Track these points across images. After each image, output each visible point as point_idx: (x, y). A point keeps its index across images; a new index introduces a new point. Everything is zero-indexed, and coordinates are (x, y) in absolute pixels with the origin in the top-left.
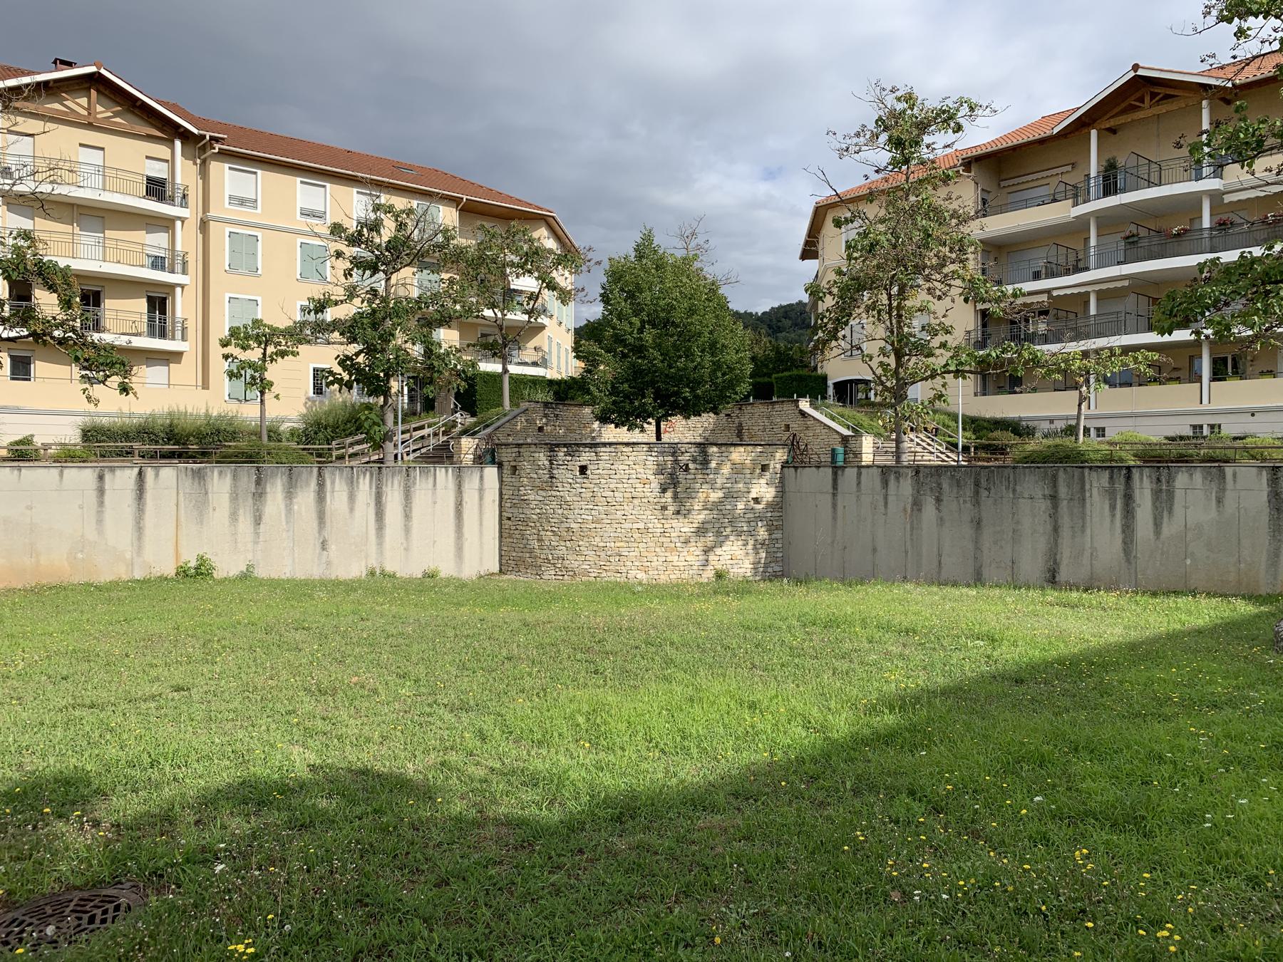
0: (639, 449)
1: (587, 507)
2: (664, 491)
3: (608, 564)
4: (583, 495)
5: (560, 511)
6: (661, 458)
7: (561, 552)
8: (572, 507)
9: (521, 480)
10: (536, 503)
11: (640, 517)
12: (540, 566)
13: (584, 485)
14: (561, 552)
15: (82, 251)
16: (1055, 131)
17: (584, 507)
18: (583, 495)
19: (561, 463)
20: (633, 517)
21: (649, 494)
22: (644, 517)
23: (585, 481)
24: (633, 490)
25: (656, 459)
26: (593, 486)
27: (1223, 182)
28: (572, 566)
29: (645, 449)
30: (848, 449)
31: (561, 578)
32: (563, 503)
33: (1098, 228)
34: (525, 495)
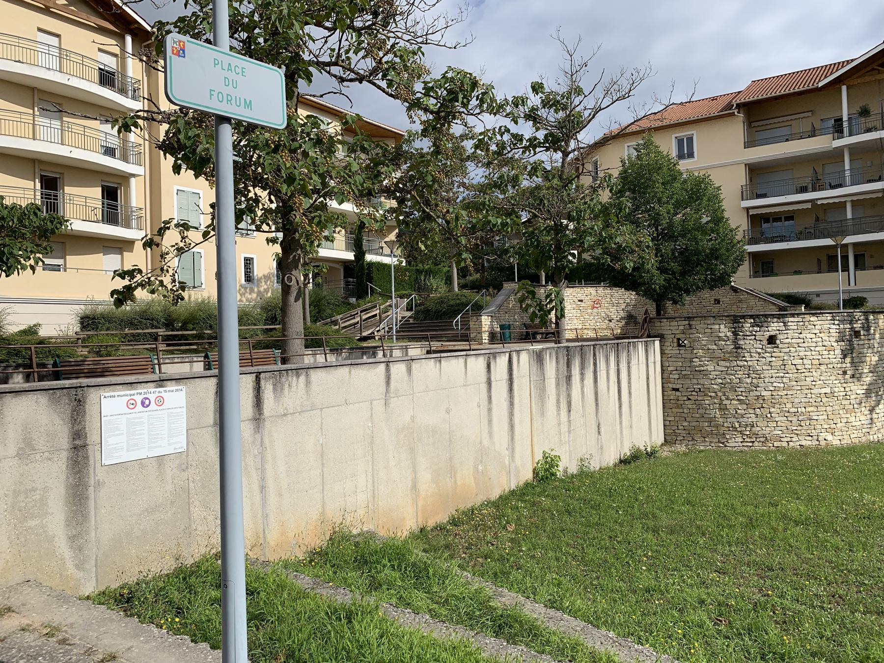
0: (823, 318)
1: (778, 375)
2: (845, 357)
3: (800, 428)
4: (773, 364)
5: (749, 381)
6: (842, 326)
7: (750, 420)
8: (762, 376)
9: (695, 351)
10: (717, 373)
11: (827, 382)
12: (724, 434)
13: (774, 354)
14: (750, 420)
15: (41, 132)
16: (820, 85)
17: (774, 375)
18: (773, 364)
19: (748, 333)
20: (821, 382)
21: (834, 360)
22: (831, 382)
23: (775, 350)
24: (820, 357)
25: (838, 327)
26: (782, 354)
28: (764, 432)
29: (829, 318)
31: (750, 444)
32: (750, 371)
33: (850, 155)
34: (700, 366)
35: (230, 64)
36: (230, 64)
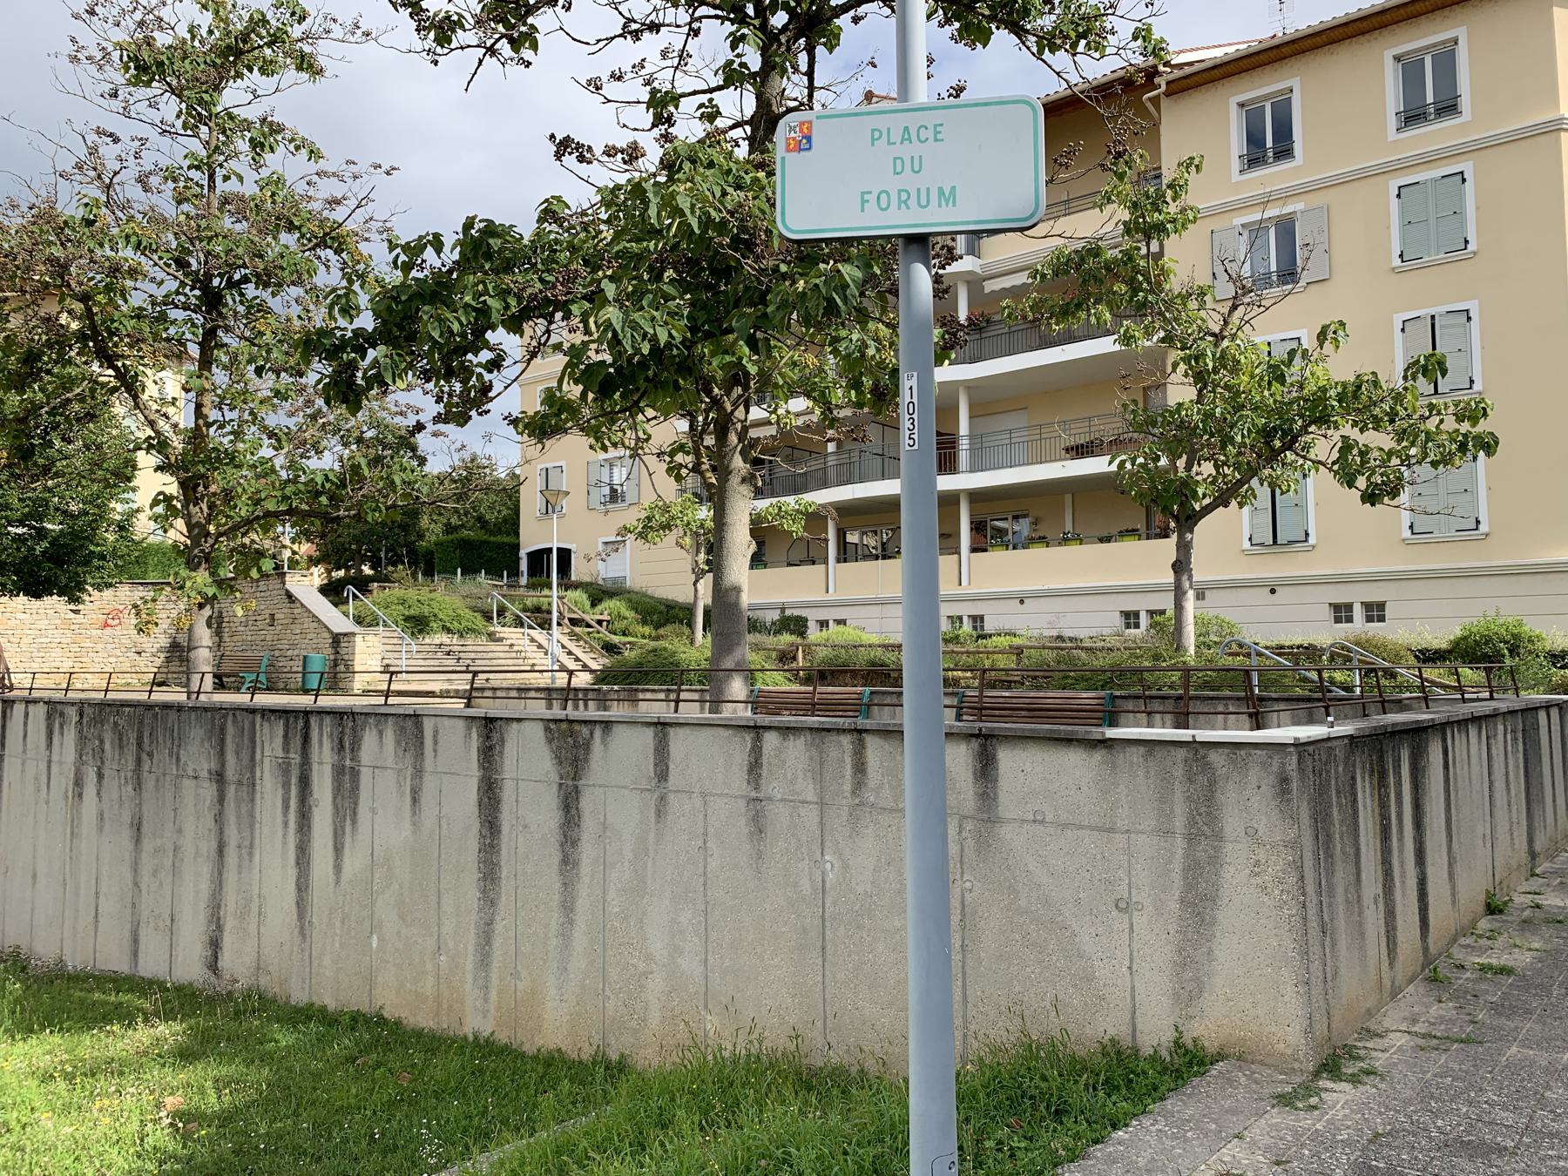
27: (980, 262)
30: (339, 657)
35: (906, 129)
36: (906, 129)
